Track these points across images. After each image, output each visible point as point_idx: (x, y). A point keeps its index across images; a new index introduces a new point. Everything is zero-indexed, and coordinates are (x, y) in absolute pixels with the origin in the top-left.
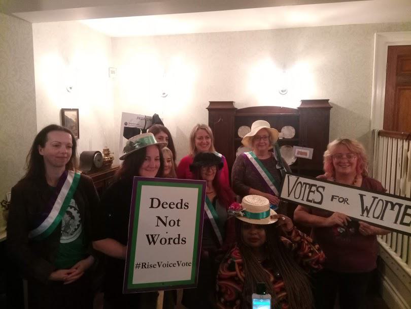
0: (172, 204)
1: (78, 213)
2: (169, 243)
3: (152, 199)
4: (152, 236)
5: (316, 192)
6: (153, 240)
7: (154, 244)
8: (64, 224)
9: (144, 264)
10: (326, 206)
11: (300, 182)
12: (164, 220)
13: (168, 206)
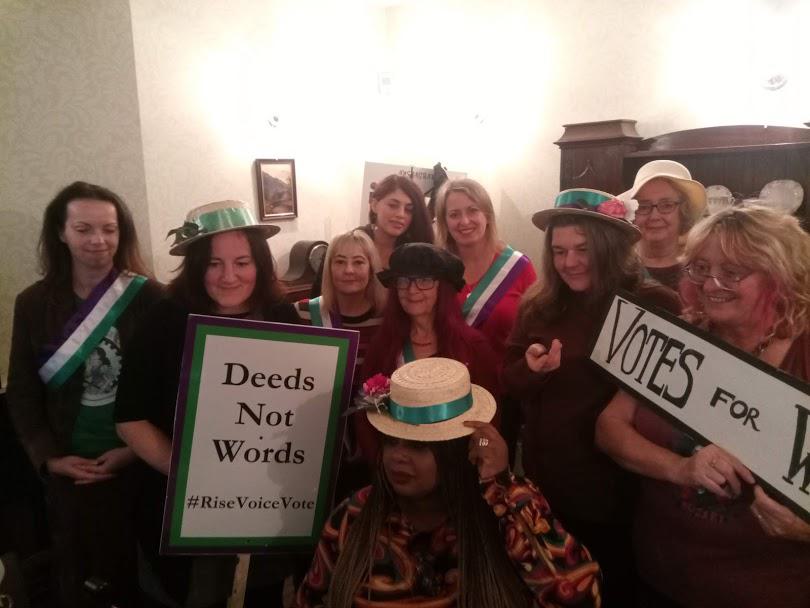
0: (276, 377)
1: (117, 354)
2: (266, 460)
3: (230, 366)
4: (227, 443)
5: (677, 363)
6: (229, 452)
7: (231, 460)
8: (89, 368)
9: (207, 500)
10: (696, 416)
11: (644, 327)
12: (256, 411)
13: (265, 382)
